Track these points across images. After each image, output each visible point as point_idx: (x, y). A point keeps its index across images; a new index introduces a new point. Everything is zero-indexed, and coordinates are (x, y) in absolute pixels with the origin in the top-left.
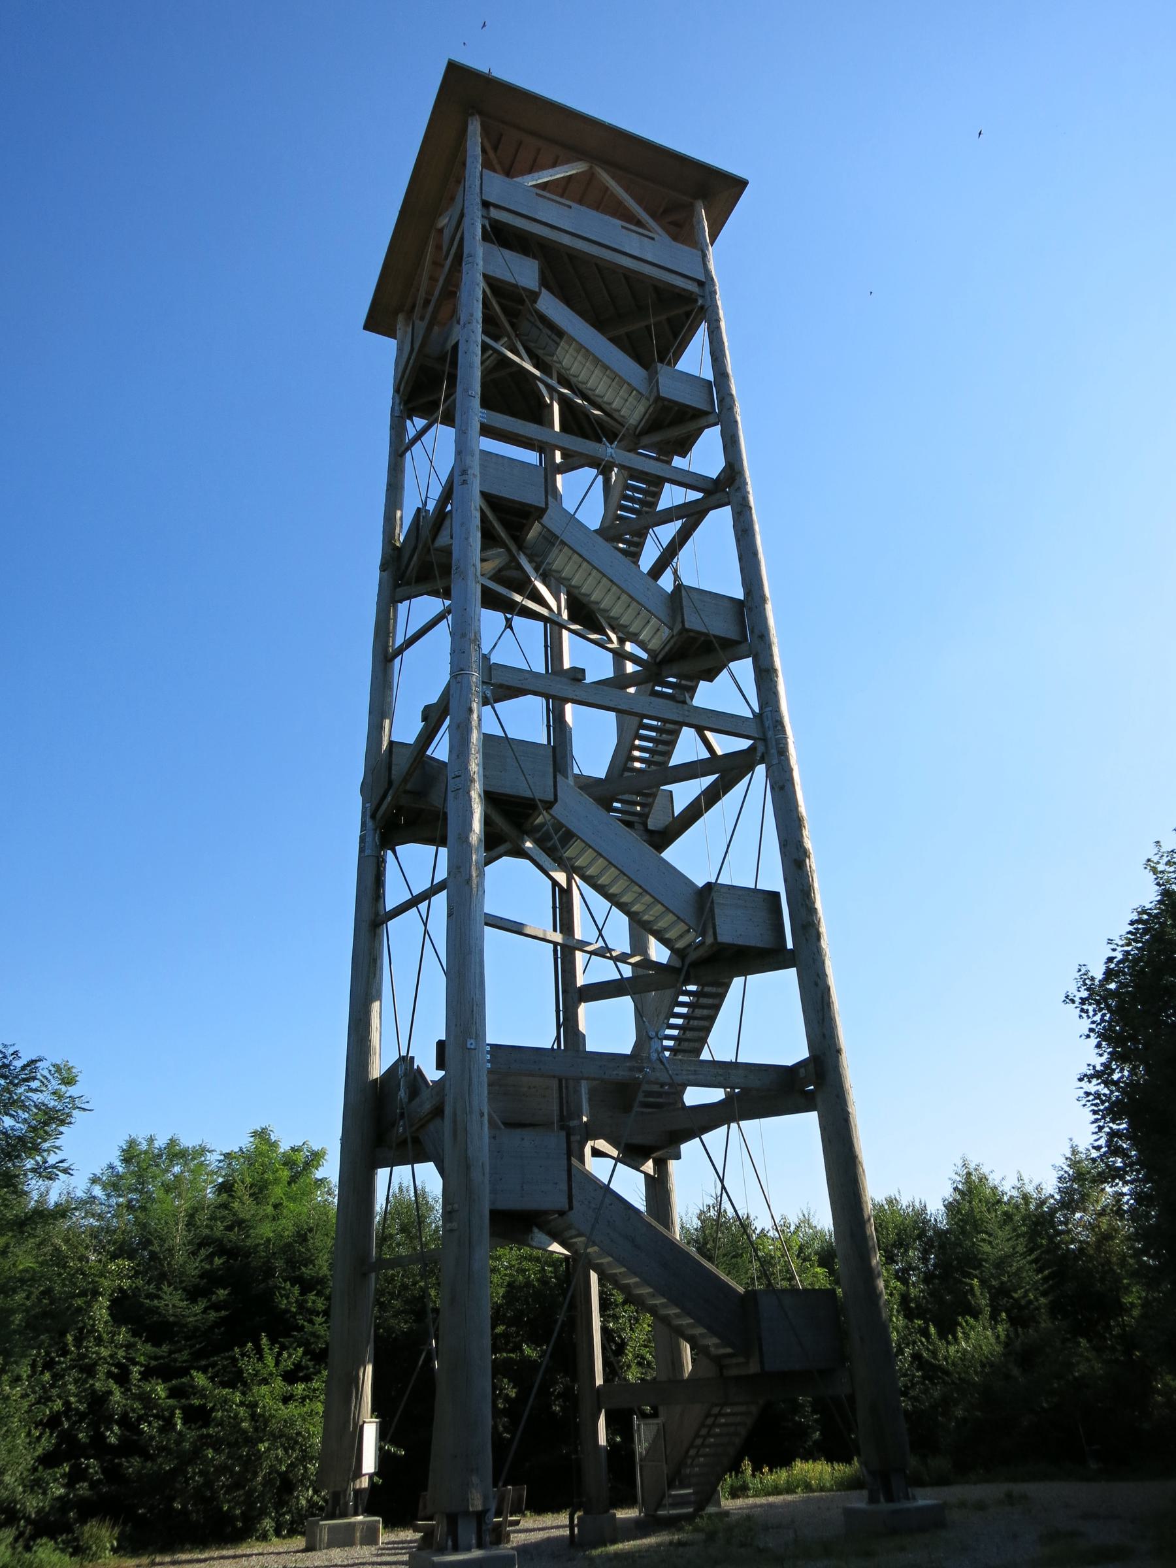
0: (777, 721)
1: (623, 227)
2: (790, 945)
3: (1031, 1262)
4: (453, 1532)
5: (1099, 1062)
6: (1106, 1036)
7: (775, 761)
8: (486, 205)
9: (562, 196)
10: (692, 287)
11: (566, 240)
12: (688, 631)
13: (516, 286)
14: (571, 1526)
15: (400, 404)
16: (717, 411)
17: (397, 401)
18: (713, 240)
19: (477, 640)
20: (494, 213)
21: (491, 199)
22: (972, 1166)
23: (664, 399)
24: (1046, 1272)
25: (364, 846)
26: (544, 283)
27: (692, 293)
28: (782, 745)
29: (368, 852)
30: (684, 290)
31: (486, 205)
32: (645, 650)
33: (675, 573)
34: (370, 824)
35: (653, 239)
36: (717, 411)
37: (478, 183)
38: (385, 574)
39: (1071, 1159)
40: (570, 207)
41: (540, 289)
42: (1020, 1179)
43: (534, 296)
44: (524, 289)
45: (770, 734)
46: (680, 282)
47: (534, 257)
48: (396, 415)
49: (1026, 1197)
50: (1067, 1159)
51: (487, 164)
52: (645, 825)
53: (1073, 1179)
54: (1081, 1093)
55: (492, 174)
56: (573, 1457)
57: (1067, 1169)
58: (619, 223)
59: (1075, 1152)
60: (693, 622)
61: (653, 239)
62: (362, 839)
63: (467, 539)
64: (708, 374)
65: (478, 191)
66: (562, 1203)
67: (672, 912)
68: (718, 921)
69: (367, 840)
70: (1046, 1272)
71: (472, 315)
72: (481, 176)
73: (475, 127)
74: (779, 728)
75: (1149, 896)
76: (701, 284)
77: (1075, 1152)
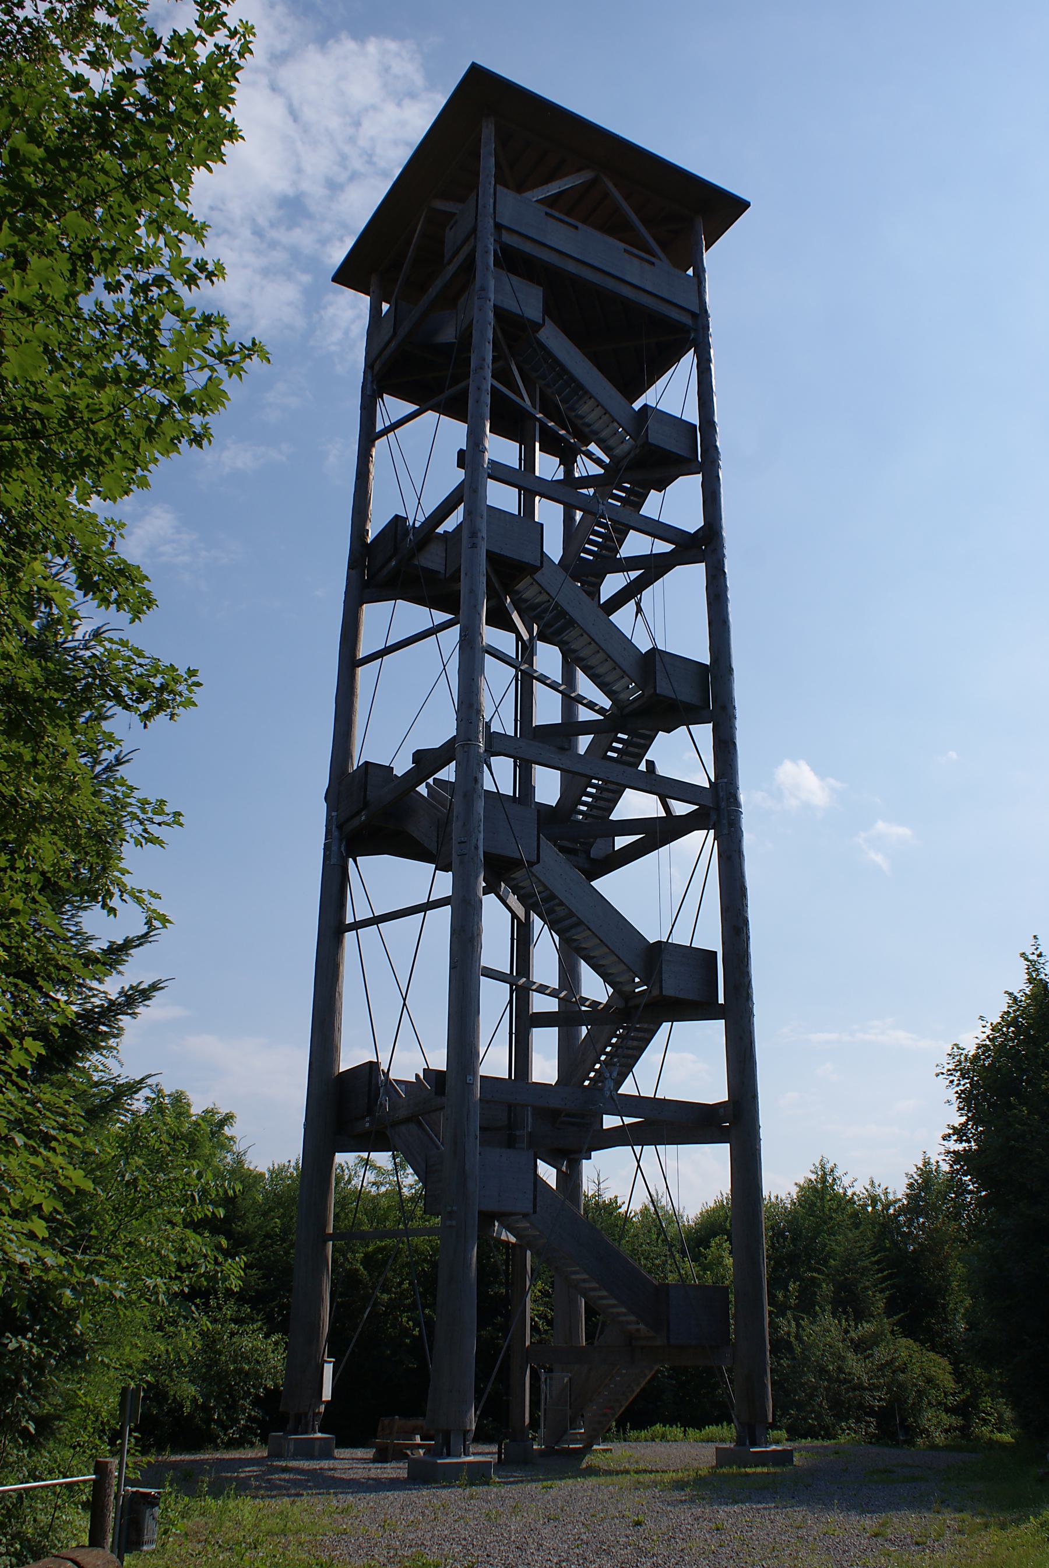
0: (731, 793)
1: (625, 251)
2: (721, 1001)
3: (873, 1263)
4: (447, 1443)
5: (958, 1120)
6: (967, 1099)
7: (725, 831)
8: (498, 227)
9: (567, 214)
10: (687, 320)
11: (571, 267)
12: (658, 695)
13: (522, 317)
14: (500, 1453)
15: (372, 382)
16: (700, 459)
17: (370, 378)
18: (706, 250)
19: (479, 712)
20: (507, 238)
21: (505, 222)
22: (829, 1166)
23: (651, 444)
24: (885, 1273)
25: (330, 854)
26: (547, 311)
27: (685, 325)
28: (733, 817)
29: (333, 861)
30: (678, 321)
31: (498, 227)
32: (609, 694)
33: (638, 604)
34: (336, 833)
35: (653, 264)
36: (700, 459)
37: (492, 201)
38: (353, 572)
39: (922, 1170)
40: (577, 228)
41: (544, 320)
42: (872, 1183)
43: (538, 326)
44: (529, 320)
45: (723, 804)
46: (675, 314)
47: (539, 284)
48: (368, 393)
49: (874, 1200)
50: (918, 1169)
51: (500, 180)
52: (588, 853)
53: (921, 1188)
54: (942, 1150)
55: (505, 190)
56: (505, 1398)
57: (917, 1178)
58: (622, 245)
59: (927, 1163)
60: (663, 687)
61: (653, 264)
62: (327, 847)
63: (475, 606)
64: (693, 417)
65: (492, 210)
66: (528, 1207)
67: (625, 964)
68: (665, 977)
69: (333, 848)
70: (885, 1273)
71: (484, 360)
72: (495, 190)
73: (488, 131)
74: (732, 800)
75: (1019, 984)
76: (694, 315)
77: (927, 1163)
